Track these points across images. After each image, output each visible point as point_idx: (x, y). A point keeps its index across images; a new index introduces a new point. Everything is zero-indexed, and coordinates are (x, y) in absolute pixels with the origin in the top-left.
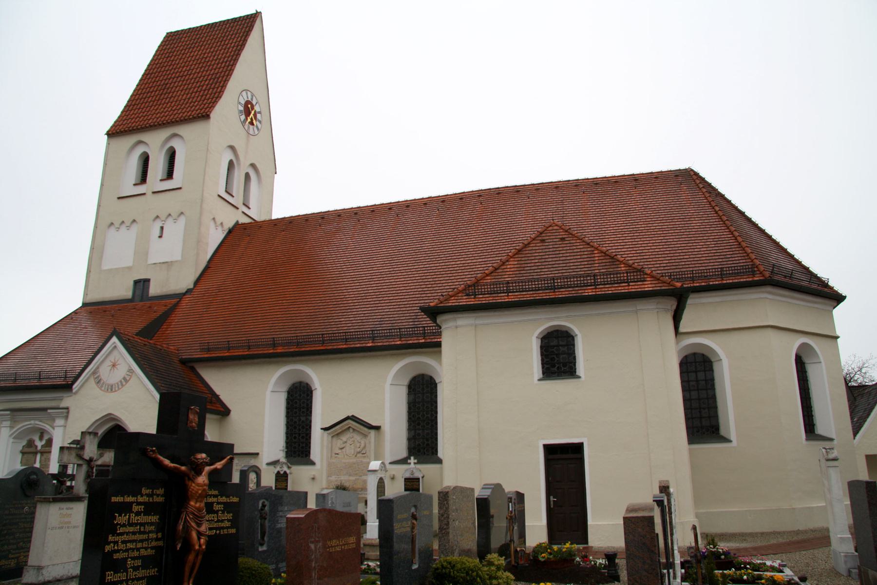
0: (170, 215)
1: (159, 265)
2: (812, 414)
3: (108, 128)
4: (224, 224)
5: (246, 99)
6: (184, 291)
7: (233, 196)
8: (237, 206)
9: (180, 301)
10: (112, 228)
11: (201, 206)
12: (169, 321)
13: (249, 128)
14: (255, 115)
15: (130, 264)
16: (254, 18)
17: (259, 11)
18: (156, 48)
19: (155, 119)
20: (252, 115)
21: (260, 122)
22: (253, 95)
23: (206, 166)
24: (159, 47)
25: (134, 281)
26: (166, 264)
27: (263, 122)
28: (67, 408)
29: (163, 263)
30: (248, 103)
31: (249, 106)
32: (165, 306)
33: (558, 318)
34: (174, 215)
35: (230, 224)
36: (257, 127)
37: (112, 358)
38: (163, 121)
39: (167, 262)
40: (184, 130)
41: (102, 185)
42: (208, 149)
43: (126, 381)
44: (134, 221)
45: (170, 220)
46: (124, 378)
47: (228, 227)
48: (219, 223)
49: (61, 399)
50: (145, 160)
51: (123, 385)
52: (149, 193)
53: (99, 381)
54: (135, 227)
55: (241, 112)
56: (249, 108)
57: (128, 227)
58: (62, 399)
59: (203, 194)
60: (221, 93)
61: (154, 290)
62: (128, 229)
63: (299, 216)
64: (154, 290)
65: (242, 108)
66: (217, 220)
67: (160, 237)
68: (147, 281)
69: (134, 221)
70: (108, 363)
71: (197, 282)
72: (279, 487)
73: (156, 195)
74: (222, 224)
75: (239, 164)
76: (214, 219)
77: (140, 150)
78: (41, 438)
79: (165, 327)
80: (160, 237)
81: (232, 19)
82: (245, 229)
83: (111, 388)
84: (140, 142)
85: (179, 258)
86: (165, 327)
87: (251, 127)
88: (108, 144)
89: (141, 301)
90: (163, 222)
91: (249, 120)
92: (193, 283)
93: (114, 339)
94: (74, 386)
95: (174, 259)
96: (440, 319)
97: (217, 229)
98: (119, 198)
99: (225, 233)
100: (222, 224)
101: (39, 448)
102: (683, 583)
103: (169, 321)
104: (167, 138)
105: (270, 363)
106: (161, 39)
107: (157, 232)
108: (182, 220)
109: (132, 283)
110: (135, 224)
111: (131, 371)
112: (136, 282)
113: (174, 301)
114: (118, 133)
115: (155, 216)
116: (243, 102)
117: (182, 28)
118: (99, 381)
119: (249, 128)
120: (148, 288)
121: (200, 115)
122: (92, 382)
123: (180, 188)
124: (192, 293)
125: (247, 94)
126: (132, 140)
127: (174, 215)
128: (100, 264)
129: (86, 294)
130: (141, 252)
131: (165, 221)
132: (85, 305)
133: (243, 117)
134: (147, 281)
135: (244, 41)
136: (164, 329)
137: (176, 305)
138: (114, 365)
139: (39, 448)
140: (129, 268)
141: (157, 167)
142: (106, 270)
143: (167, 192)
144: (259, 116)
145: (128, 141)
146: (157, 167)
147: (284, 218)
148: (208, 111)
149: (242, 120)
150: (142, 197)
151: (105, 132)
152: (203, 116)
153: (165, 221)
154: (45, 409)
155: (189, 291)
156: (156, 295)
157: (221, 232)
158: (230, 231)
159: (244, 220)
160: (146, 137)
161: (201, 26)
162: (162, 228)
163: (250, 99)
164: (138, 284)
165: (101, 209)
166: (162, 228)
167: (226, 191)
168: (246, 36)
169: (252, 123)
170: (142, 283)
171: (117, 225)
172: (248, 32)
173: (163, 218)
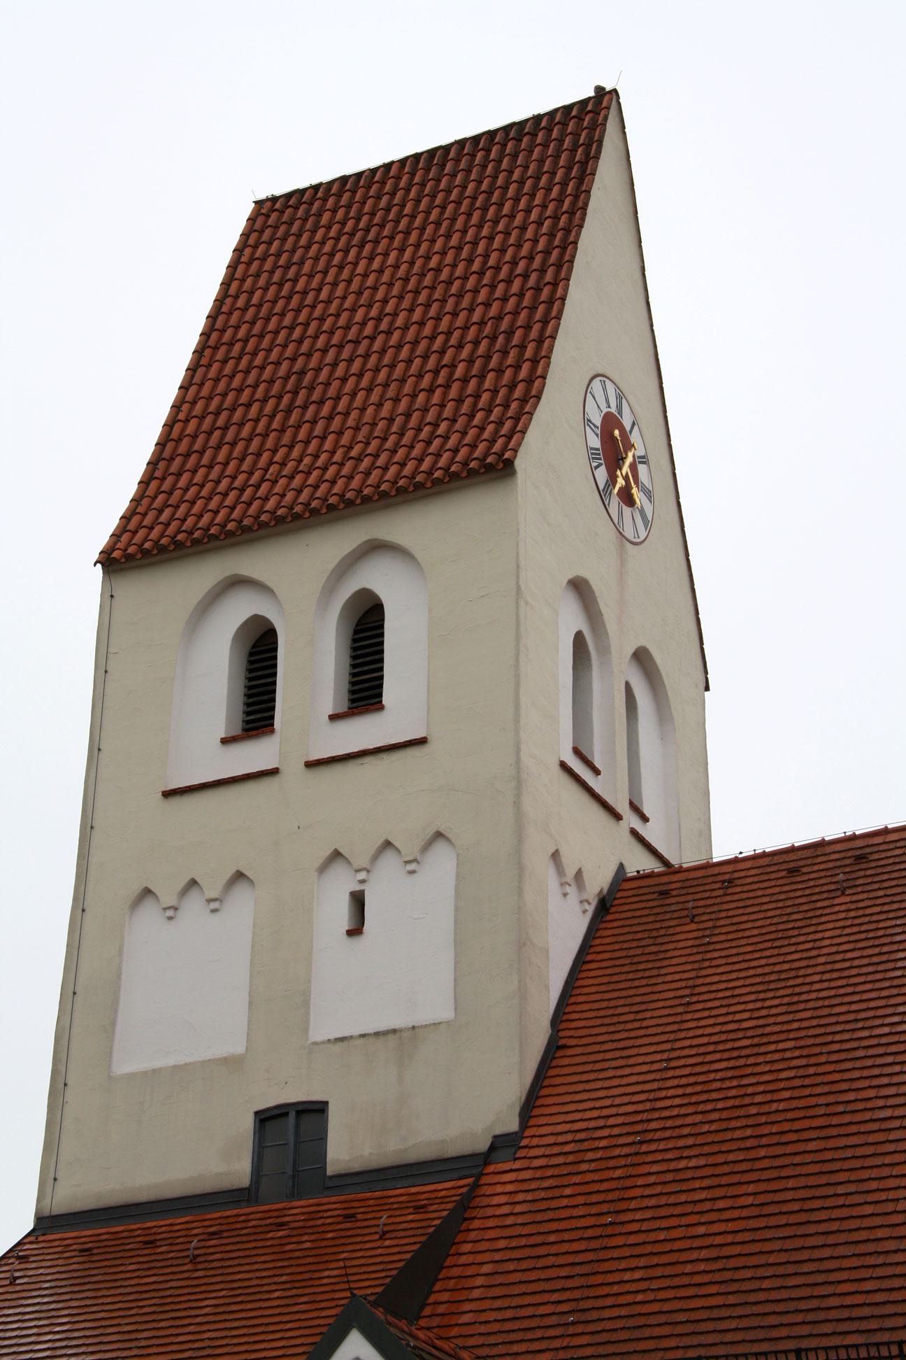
0: (147, 892)
1: (361, 1041)
3: (101, 540)
4: (586, 876)
5: (605, 410)
6: (483, 1145)
9: (476, 1186)
10: (149, 908)
11: (517, 804)
12: (455, 1272)
13: (621, 514)
14: (633, 467)
15: (237, 1047)
16: (596, 112)
18: (226, 257)
19: (142, 533)
20: (626, 469)
21: (649, 494)
22: (620, 397)
23: (517, 655)
24: (238, 251)
25: (257, 1113)
26: (392, 1040)
27: (657, 494)
29: (377, 1034)
30: (610, 422)
31: (617, 433)
32: (419, 1209)
34: (409, 847)
35: (599, 880)
36: (642, 512)
38: (223, 526)
39: (394, 1031)
41: (95, 750)
42: (518, 588)
44: (239, 876)
45: (390, 863)
47: (597, 890)
48: (570, 872)
54: (242, 904)
57: (215, 904)
59: (518, 761)
60: (537, 383)
62: (214, 911)
63: (885, 831)
65: (595, 442)
66: (565, 858)
67: (355, 931)
68: (315, 1111)
69: (239, 876)
71: (530, 1106)
73: (176, 801)
74: (579, 875)
75: (604, 650)
76: (555, 856)
79: (446, 1296)
80: (355, 931)
81: (507, 129)
82: (664, 894)
84: (237, 582)
85: (447, 1013)
86: (446, 1296)
87: (627, 511)
88: (109, 597)
89: (294, 1194)
90: (362, 875)
92: (517, 1110)
95: (422, 1016)
97: (565, 895)
98: (168, 794)
99: (591, 909)
100: (579, 875)
103: (455, 1272)
106: (240, 225)
107: (341, 915)
108: (442, 864)
109: (248, 1123)
110: (241, 891)
112: (266, 1119)
113: (451, 1188)
114: (146, 553)
115: (328, 852)
116: (598, 421)
117: (315, 181)
119: (621, 514)
120: (322, 1138)
121: (231, 526)
123: (422, 741)
124: (521, 1153)
125: (605, 389)
127: (409, 847)
128: (108, 1055)
129: (49, 1178)
131: (176, 909)
132: (46, 1223)
133: (602, 474)
134: (315, 1111)
135: (576, 197)
136: (442, 1309)
137: (465, 1207)
140: (232, 1063)
142: (132, 1077)
143: (368, 760)
144: (642, 469)
147: (822, 844)
148: (505, 448)
149: (601, 486)
151: (96, 556)
152: (489, 468)
153: (176, 909)
155: (502, 1144)
156: (356, 1167)
157: (577, 909)
158: (604, 906)
159: (639, 863)
160: (252, 561)
161: (387, 167)
162: (358, 901)
163: (613, 410)
164: (270, 1126)
165: (97, 837)
166: (358, 901)
167: (577, 752)
168: (581, 180)
169: (627, 498)
170: (292, 1115)
172: (584, 164)
173: (362, 861)
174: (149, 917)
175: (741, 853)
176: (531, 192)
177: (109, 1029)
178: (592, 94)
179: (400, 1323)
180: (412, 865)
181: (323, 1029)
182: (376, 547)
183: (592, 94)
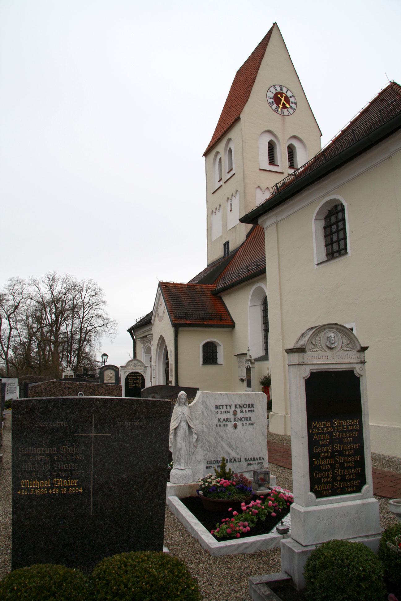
5: (275, 92)
7: (278, 166)
8: (281, 172)
17: (274, 23)
21: (294, 103)
26: (234, 228)
33: (328, 193)
55: (271, 103)
56: (279, 97)
58: (151, 330)
75: (278, 141)
76: (259, 187)
80: (231, 211)
87: (285, 110)
91: (281, 106)
96: (260, 221)
98: (213, 193)
102: (8, 413)
104: (226, 144)
116: (272, 95)
133: (275, 106)
153: (232, 199)
162: (231, 204)
166: (231, 204)
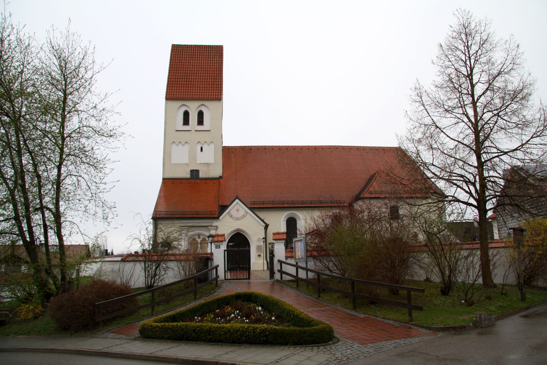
2: (175, 359)
6: (218, 177)
28: (217, 226)
37: (236, 207)
40: (208, 103)
41: (165, 123)
43: (245, 216)
45: (206, 144)
46: (244, 215)
49: (213, 223)
50: (186, 115)
51: (243, 218)
52: (193, 131)
53: (231, 216)
61: (201, 175)
64: (201, 175)
68: (197, 171)
70: (234, 209)
72: (288, 256)
73: (197, 132)
77: (184, 109)
78: (199, 238)
83: (238, 219)
84: (184, 105)
85: (213, 162)
93: (237, 200)
94: (220, 218)
98: (176, 131)
101: (199, 242)
105: (282, 210)
109: (189, 171)
110: (186, 144)
111: (247, 212)
112: (192, 171)
118: (231, 216)
122: (228, 216)
126: (180, 103)
129: (163, 174)
130: (193, 157)
134: (197, 171)
138: (238, 210)
139: (199, 242)
140: (187, 164)
141: (193, 118)
145: (178, 104)
146: (193, 118)
150: (189, 132)
154: (207, 226)
171: (177, 143)
174: (174, 146)
175: (309, 358)
176: (406, 310)
177: (170, 158)
178: (188, 176)
179: (193, 324)
180: (209, 145)
181: (198, 162)
182: (203, 105)
183: (188, 176)
